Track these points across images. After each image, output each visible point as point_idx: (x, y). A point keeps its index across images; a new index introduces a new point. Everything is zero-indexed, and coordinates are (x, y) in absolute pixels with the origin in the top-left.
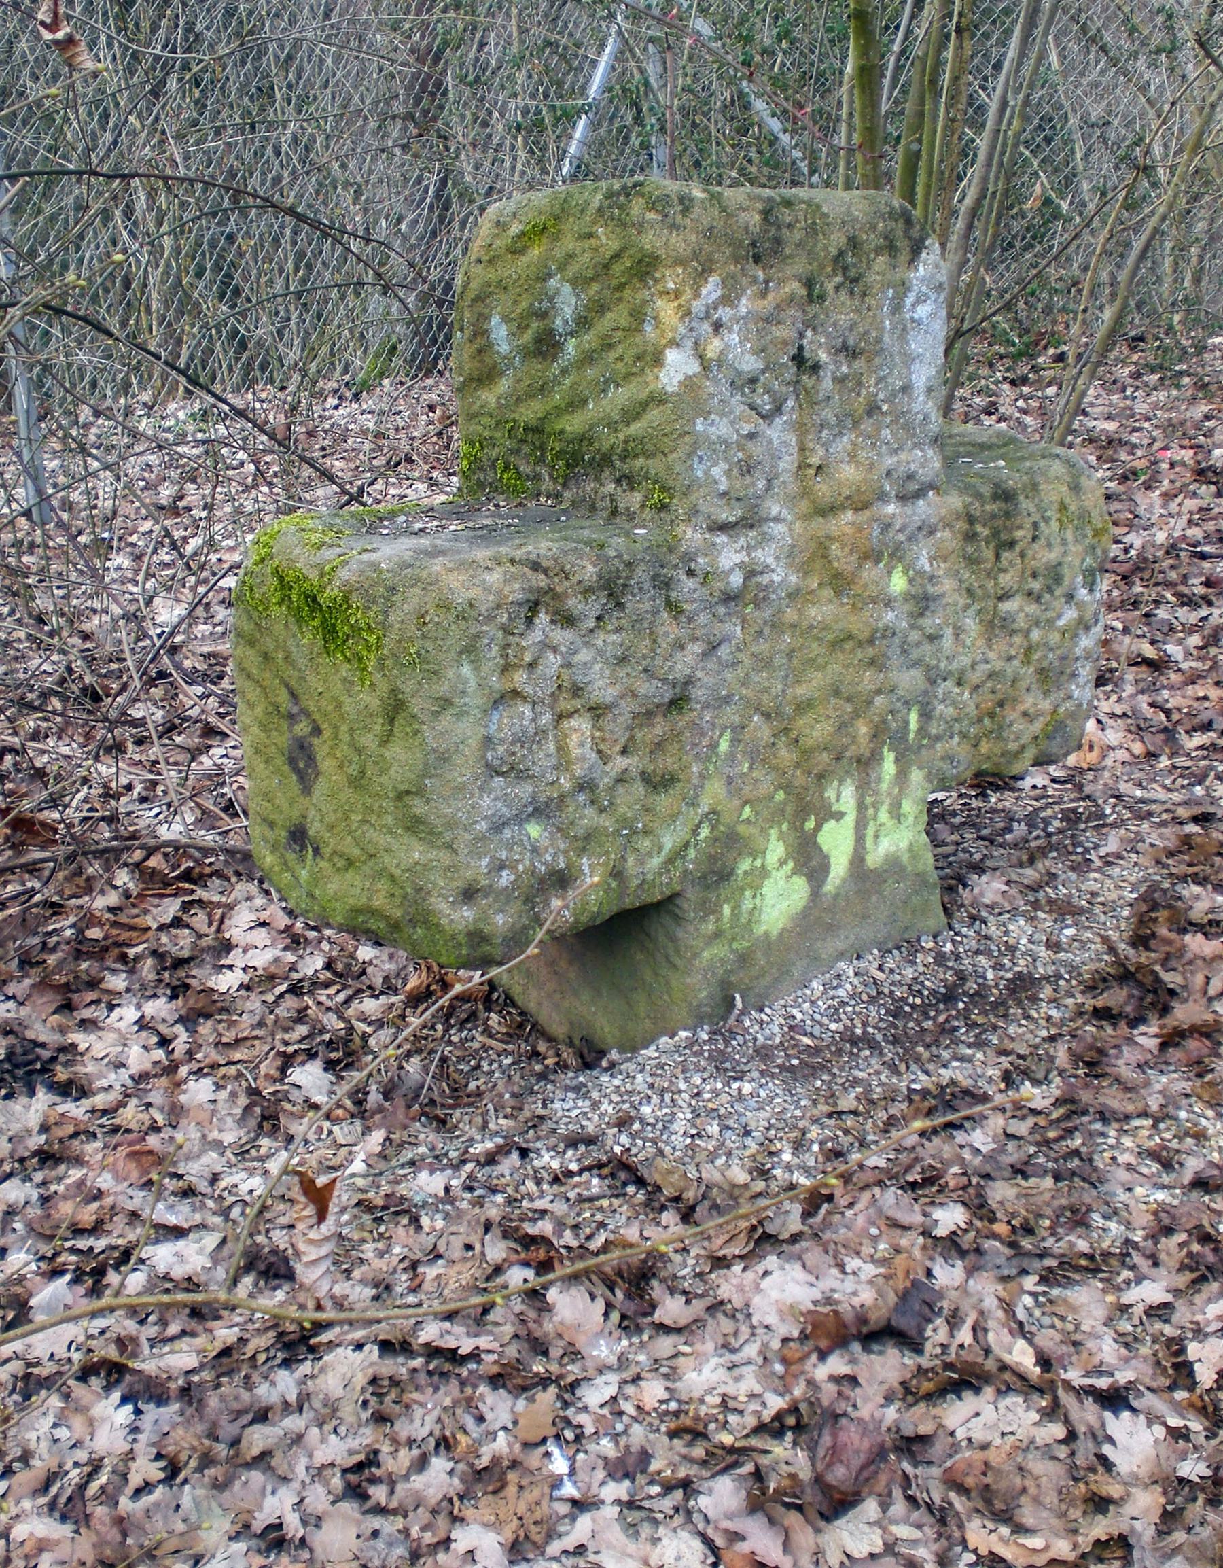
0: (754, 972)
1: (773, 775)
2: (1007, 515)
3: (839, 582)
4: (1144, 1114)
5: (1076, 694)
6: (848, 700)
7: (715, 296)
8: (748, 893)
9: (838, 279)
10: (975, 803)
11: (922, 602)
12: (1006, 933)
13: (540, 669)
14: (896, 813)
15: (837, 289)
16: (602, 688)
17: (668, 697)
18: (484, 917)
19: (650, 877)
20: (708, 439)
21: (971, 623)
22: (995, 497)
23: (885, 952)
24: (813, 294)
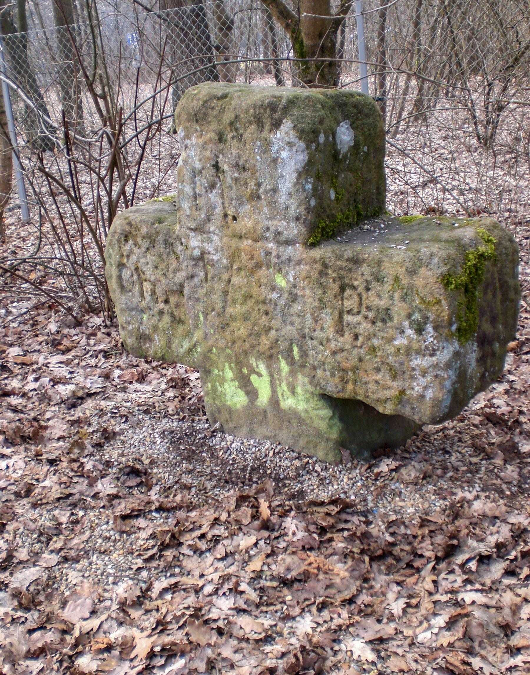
2: (350, 270)
14: (293, 392)
15: (233, 138)
16: (149, 273)
21: (328, 320)
24: (221, 139)
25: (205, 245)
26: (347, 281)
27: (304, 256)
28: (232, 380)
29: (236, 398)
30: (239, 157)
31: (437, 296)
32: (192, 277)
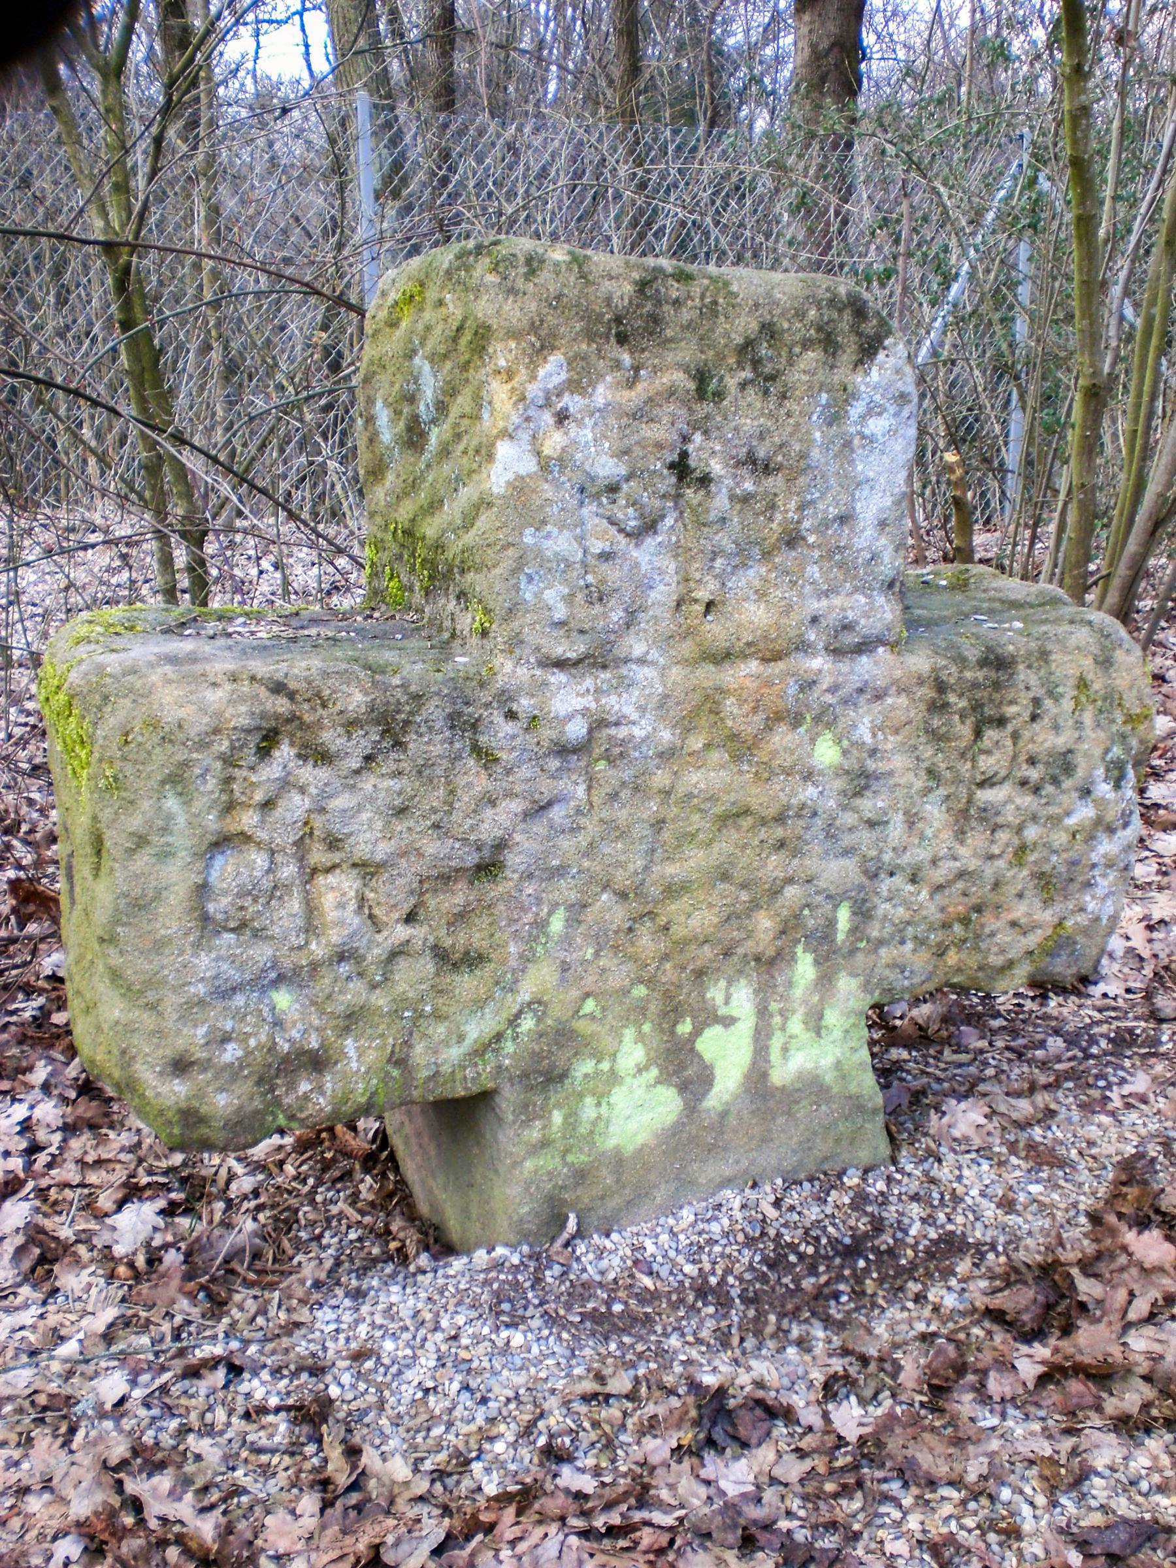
0: (597, 1191)
1: (630, 966)
2: (997, 685)
3: (740, 748)
4: (956, 1483)
5: (1091, 906)
6: (744, 886)
7: (556, 380)
8: (589, 1101)
9: (747, 374)
10: (1029, 1005)
11: (861, 781)
12: (959, 1178)
13: (278, 812)
14: (815, 1023)
16: (369, 838)
17: (472, 859)
18: (200, 1095)
19: (446, 1069)
20: (539, 554)
21: (935, 813)
22: (983, 663)
23: (792, 1182)
24: (704, 384)
26: (989, 711)
27: (898, 673)
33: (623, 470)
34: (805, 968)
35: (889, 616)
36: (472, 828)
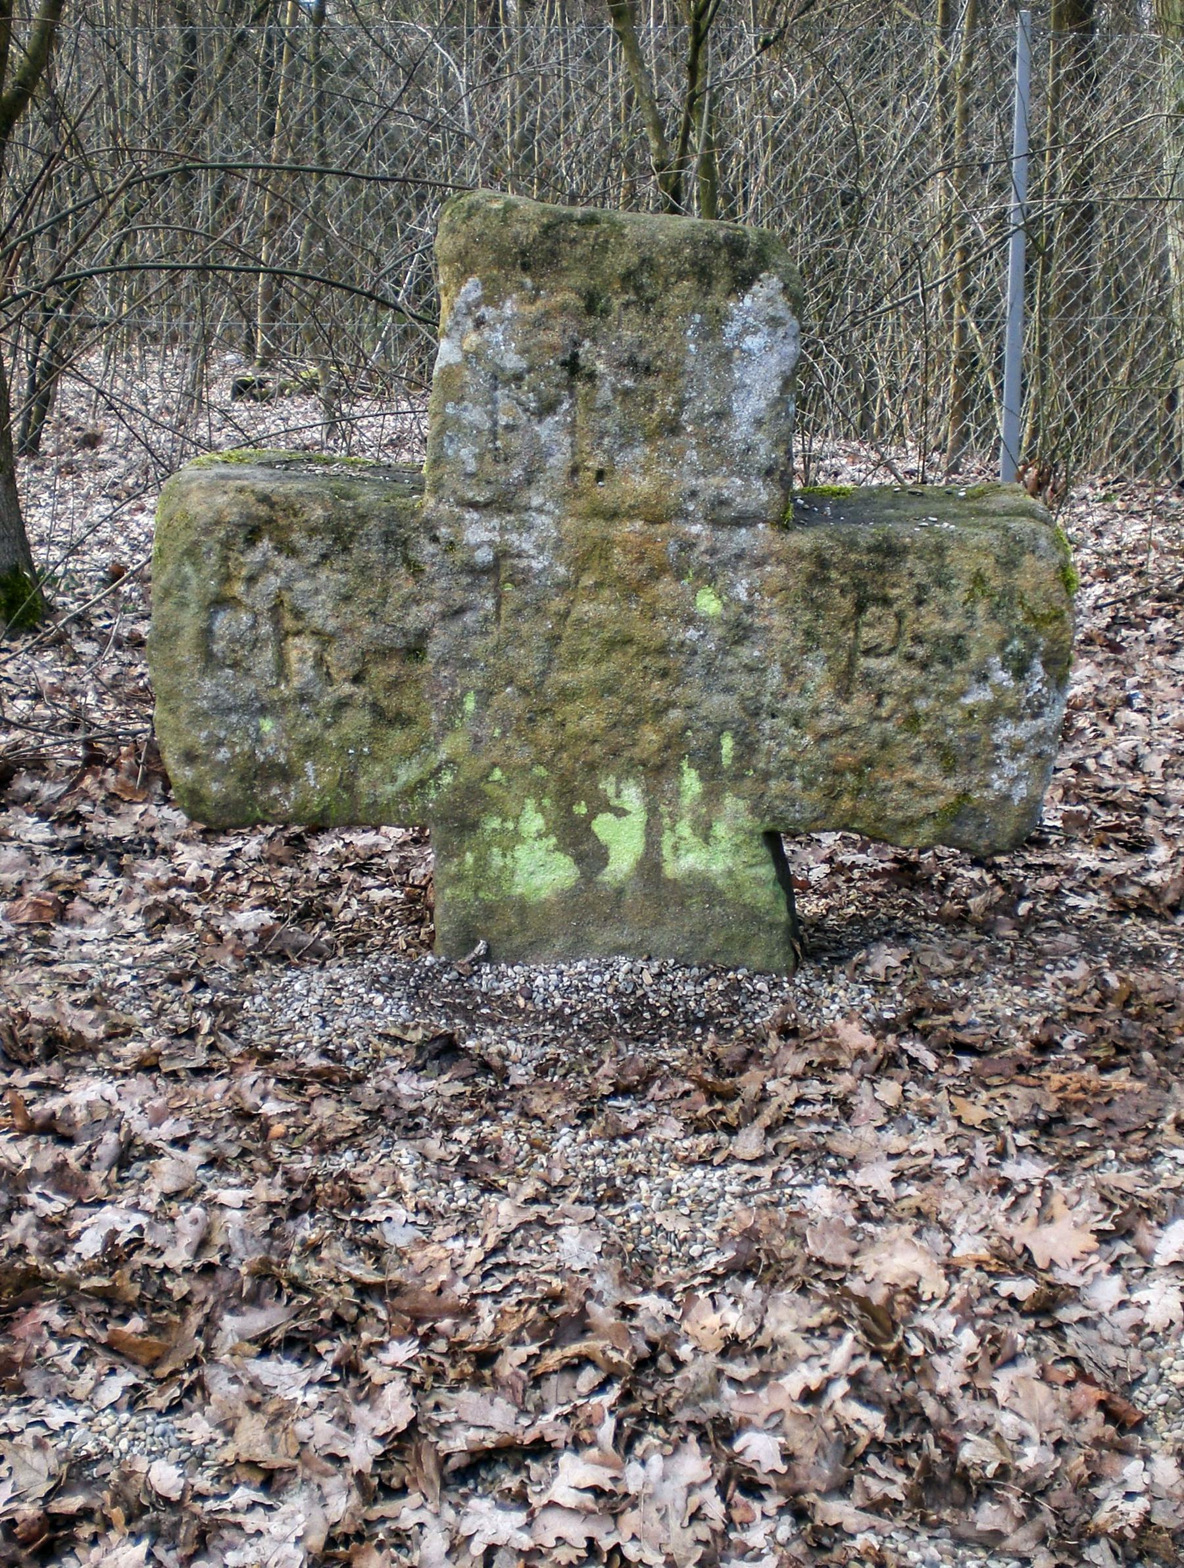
2: (881, 569)
3: (632, 590)
11: (740, 632)
14: (705, 832)
16: (321, 614)
17: (400, 642)
18: (200, 780)
20: (458, 420)
21: (817, 671)
24: (592, 304)
25: (513, 537)
26: (871, 590)
27: (777, 547)
28: (540, 836)
29: (538, 869)
30: (641, 345)
31: (1056, 604)
32: (460, 611)
33: (524, 364)
34: (691, 782)
35: (764, 497)
36: (399, 619)
